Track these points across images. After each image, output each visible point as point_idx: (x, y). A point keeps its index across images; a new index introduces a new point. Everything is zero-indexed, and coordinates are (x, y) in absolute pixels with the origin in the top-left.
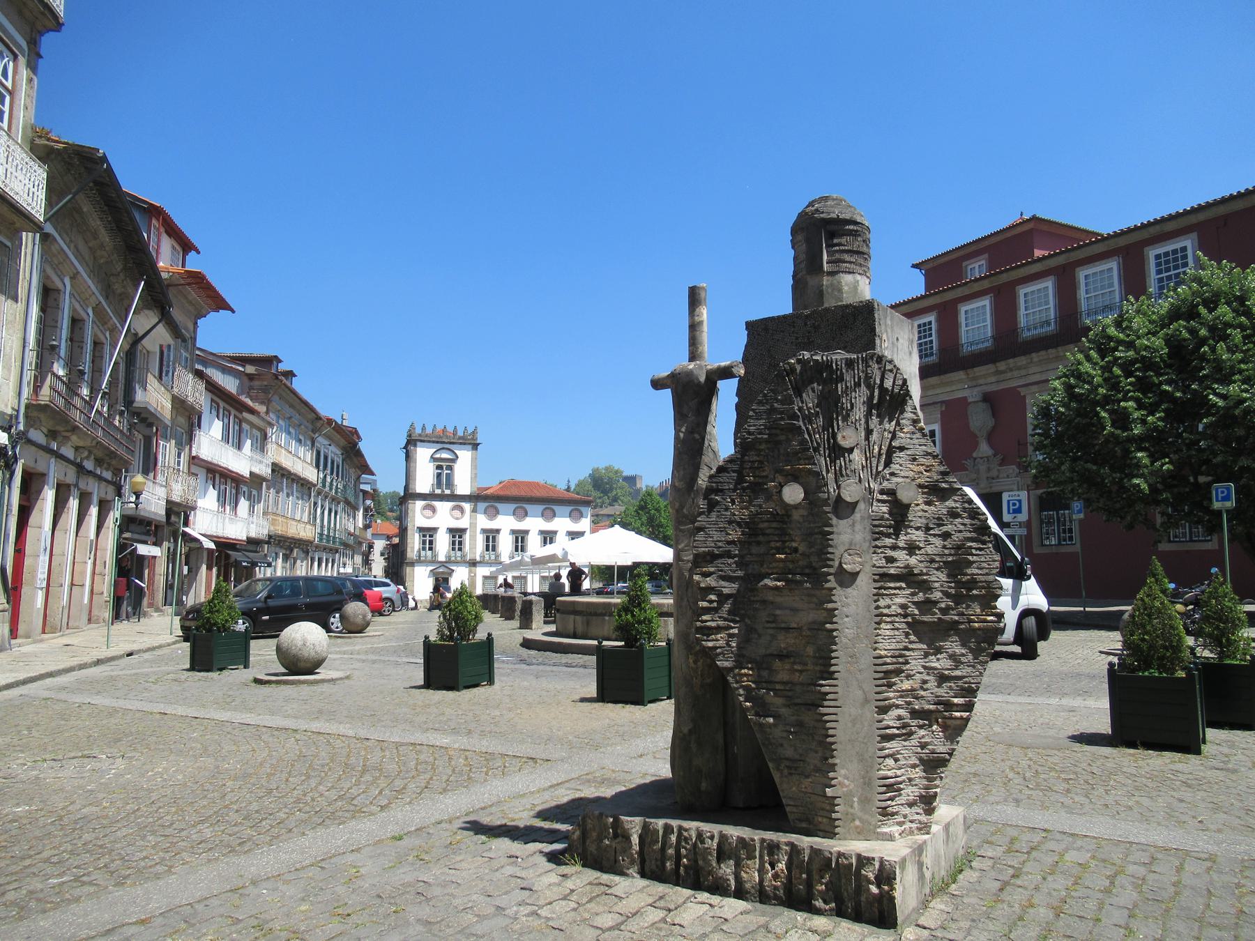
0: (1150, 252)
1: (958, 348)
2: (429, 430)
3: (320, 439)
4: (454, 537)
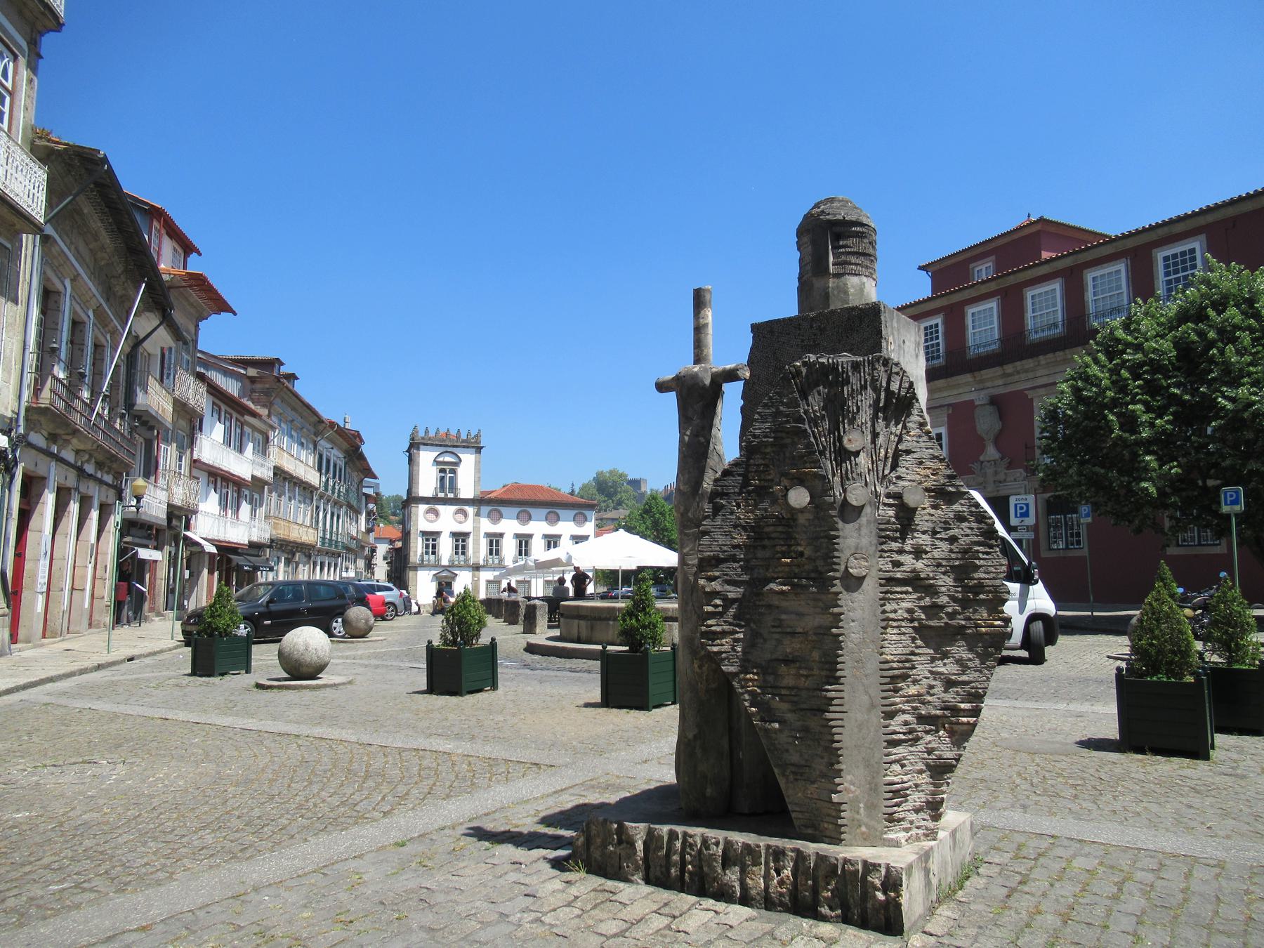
0: (1159, 254)
1: (965, 351)
2: (432, 434)
3: (322, 442)
4: (457, 541)
